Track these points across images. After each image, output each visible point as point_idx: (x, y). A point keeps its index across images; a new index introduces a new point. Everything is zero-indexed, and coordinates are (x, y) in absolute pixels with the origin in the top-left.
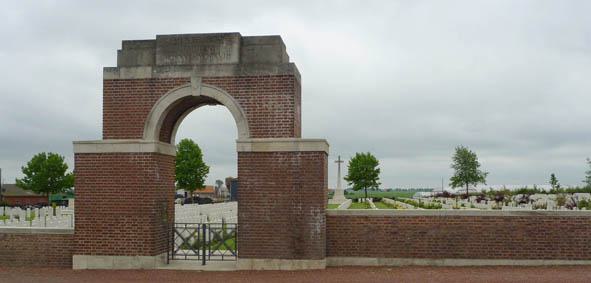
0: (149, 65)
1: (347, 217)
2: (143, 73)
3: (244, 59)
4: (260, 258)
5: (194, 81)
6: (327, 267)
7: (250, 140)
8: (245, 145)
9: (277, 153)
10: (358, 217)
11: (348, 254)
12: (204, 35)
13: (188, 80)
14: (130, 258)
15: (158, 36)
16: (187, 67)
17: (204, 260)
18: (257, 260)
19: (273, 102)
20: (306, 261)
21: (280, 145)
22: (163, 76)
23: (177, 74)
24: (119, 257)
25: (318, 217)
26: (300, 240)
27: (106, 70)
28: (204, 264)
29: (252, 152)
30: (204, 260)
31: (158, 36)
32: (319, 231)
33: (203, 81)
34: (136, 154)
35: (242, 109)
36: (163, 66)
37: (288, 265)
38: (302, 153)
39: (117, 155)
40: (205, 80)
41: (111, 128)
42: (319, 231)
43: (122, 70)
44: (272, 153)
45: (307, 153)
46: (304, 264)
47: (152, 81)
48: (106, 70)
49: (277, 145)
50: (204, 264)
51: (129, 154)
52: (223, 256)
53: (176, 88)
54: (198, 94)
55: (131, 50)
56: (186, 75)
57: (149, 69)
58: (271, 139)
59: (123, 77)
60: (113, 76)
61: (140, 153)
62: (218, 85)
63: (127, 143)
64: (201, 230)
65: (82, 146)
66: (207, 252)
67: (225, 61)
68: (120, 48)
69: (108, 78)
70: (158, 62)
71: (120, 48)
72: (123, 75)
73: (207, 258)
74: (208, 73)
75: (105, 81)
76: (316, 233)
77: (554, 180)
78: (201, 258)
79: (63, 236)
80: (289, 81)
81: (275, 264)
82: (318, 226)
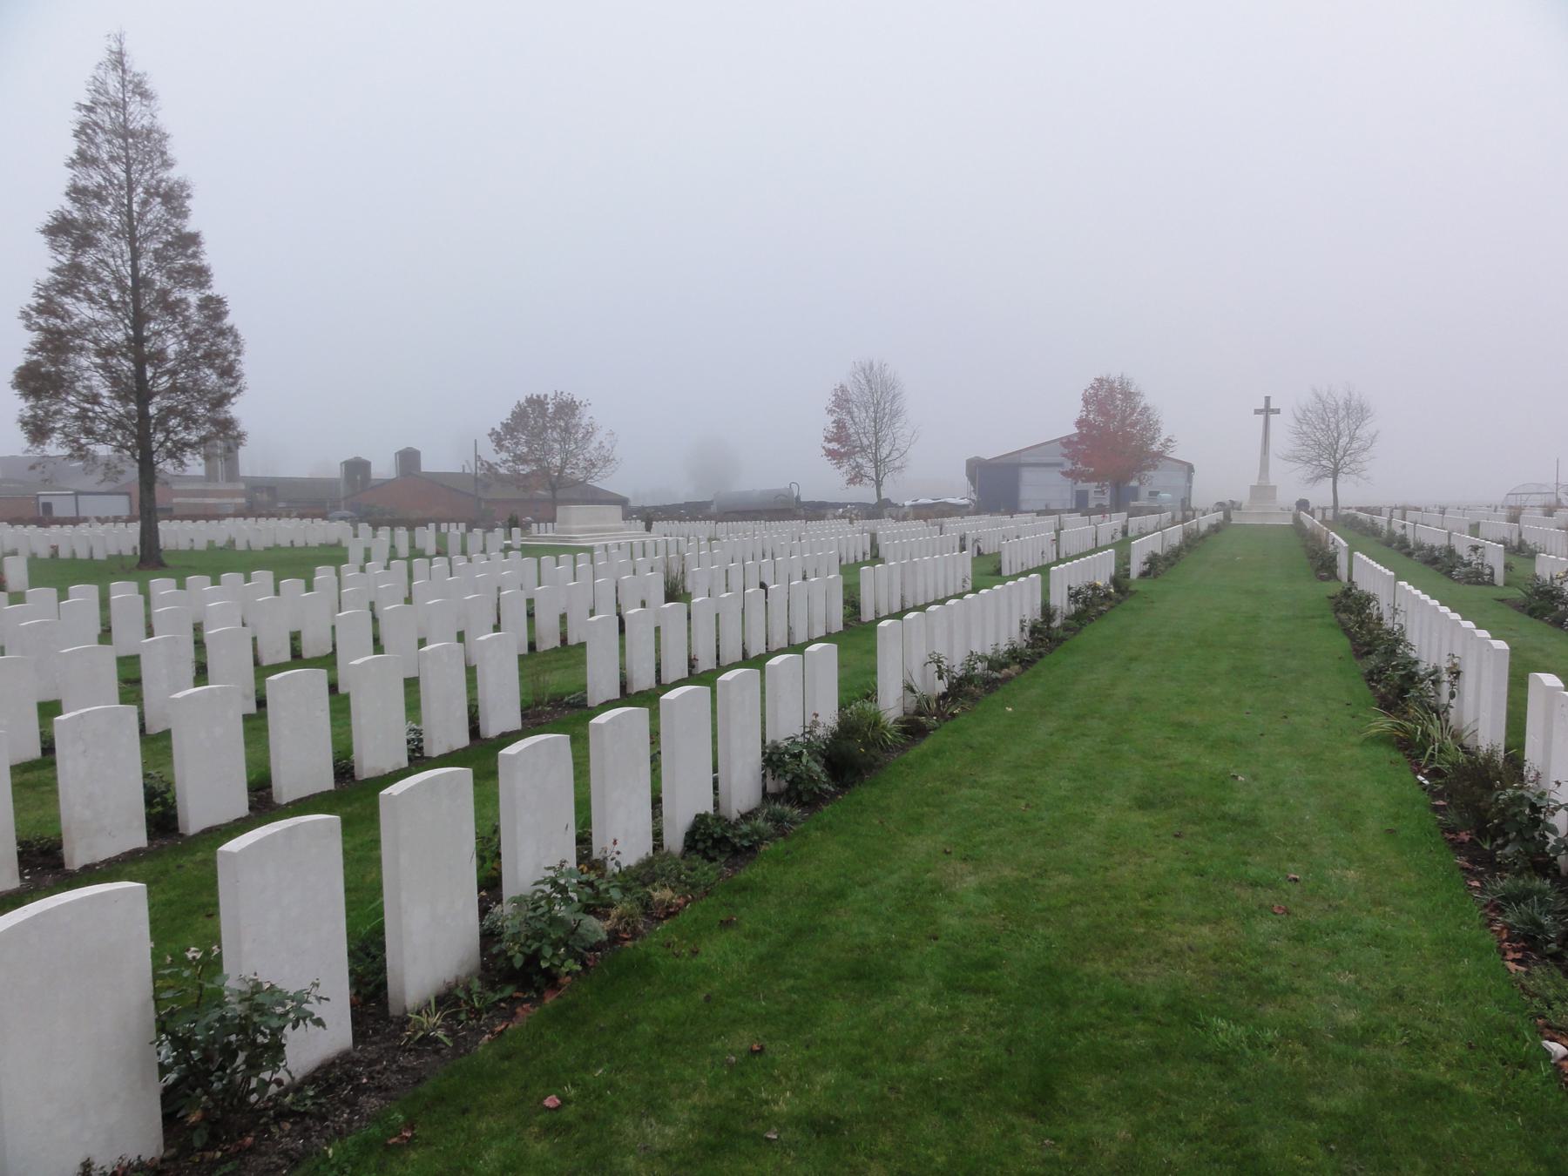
77: (1268, 399)
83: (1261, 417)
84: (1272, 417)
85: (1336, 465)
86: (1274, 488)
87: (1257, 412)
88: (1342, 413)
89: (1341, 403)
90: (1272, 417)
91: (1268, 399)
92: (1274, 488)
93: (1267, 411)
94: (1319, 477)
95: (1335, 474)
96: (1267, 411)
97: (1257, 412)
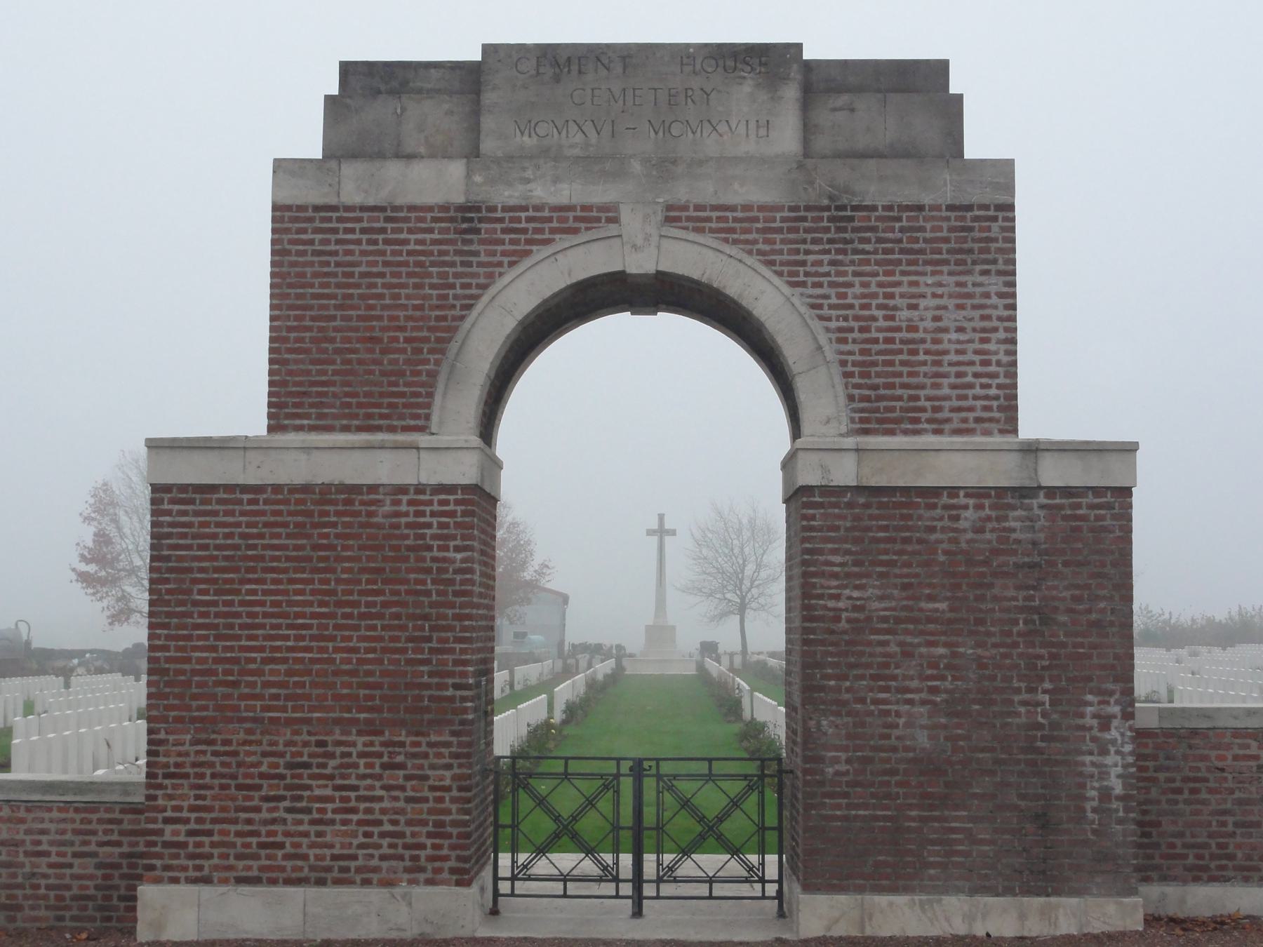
0: (462, 157)
1: (1194, 732)
2: (436, 182)
3: (822, 143)
4: (894, 890)
5: (632, 221)
6: (1152, 920)
7: (850, 442)
8: (828, 458)
9: (953, 491)
10: (1237, 733)
11: (1199, 874)
12: (670, 44)
13: (609, 214)
14: (375, 895)
15: (959, 99)
16: (592, 164)
17: (638, 899)
18: (882, 900)
19: (929, 301)
20: (1074, 901)
21: (971, 460)
22: (507, 195)
23: (566, 193)
24: (329, 892)
25: (1114, 733)
26: (1043, 821)
27: (282, 167)
28: (638, 912)
29: (859, 489)
30: (638, 899)
31: (959, 99)
32: (1118, 789)
33: (669, 220)
34: (402, 489)
35: (817, 326)
36: (510, 158)
37: (1001, 915)
38: (1051, 491)
39: (325, 494)
40: (674, 216)
41: (291, 401)
42: (1118, 789)
43: (351, 171)
44: (935, 491)
45: (1068, 492)
46: (1070, 914)
47: (467, 217)
48: (282, 167)
49: (952, 462)
50: (638, 912)
51: (373, 488)
52: (565, 879)
53: (564, 241)
54: (650, 268)
55: (371, 93)
56: (599, 194)
57: (456, 169)
58: (929, 440)
59: (352, 194)
60: (311, 193)
61: (420, 489)
62: (726, 233)
63: (369, 447)
64: (627, 785)
65: (198, 458)
66: (649, 860)
67: (749, 146)
68: (334, 90)
69: (288, 198)
70: (488, 145)
71: (334, 90)
72: (354, 186)
73: (649, 890)
74: (682, 192)
75: (278, 209)
76: (1105, 795)
77: (661, 517)
78: (627, 889)
79: (82, 806)
80: (977, 229)
81: (955, 912)
82: (1114, 769)
83: (654, 540)
84: (667, 539)
85: (743, 598)
86: (673, 628)
87: (650, 532)
88: (746, 534)
89: (745, 521)
90: (667, 539)
91: (661, 517)
92: (673, 628)
93: (661, 532)
94: (723, 615)
95: (742, 609)
96: (661, 532)
97: (650, 532)
